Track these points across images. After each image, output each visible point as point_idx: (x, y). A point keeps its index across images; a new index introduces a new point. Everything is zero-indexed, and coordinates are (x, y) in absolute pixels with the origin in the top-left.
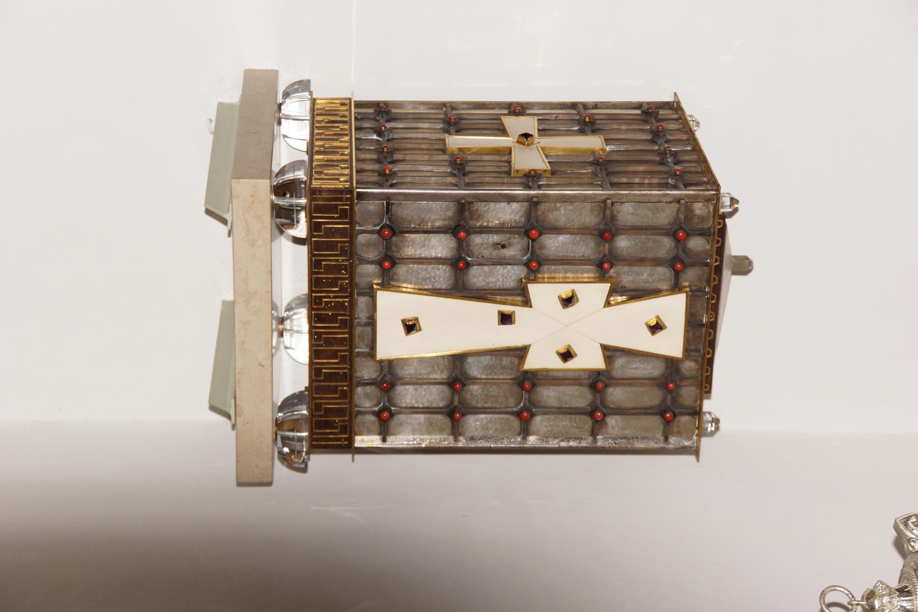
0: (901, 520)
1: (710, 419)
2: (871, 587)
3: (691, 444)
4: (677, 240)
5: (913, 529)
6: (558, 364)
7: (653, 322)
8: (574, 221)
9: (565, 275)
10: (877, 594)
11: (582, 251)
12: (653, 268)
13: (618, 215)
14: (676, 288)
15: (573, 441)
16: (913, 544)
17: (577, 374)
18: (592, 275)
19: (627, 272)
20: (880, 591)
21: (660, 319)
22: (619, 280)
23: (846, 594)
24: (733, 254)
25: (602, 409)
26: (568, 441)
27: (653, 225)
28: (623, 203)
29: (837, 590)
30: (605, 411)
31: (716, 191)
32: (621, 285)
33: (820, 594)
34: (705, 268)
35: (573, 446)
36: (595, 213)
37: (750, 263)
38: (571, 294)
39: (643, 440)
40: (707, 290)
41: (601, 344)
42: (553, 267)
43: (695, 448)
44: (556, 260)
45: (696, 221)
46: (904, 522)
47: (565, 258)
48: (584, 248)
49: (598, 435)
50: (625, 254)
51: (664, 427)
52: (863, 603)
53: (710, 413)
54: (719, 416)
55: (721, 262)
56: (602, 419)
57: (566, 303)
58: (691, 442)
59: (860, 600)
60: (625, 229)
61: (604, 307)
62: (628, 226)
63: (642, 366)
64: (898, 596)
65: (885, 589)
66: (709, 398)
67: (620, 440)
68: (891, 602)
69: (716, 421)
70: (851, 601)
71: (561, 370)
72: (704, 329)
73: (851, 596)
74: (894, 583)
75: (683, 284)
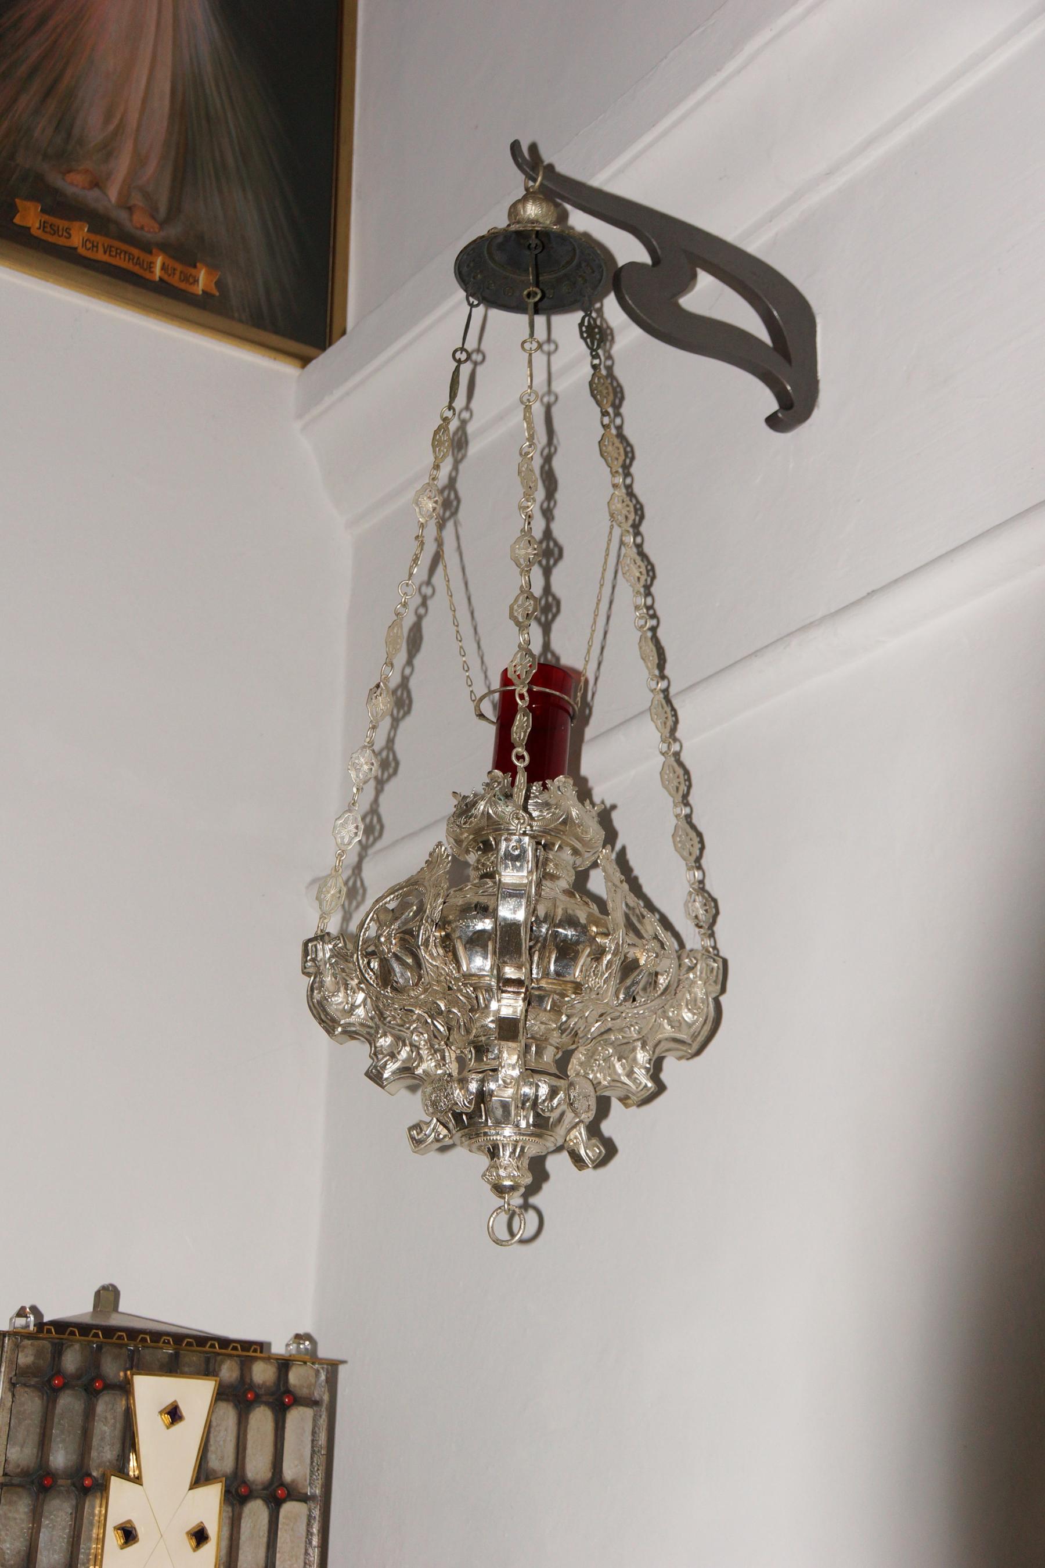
0: (415, 1147)
1: (295, 1345)
2: (489, 1187)
3: (323, 1371)
4: (64, 1386)
5: (425, 1135)
6: (210, 1550)
7: (167, 1418)
8: (23, 1528)
9: (93, 1540)
10: (497, 1182)
11: (64, 1517)
12: (96, 1418)
13: (21, 1467)
14: (126, 1389)
15: (312, 1528)
16: (441, 1136)
17: (227, 1521)
18: (98, 1502)
19: (99, 1453)
20: (494, 1178)
21: (165, 1409)
22: (108, 1464)
23: (496, 1216)
24: (91, 1309)
25: (274, 1486)
26: (312, 1534)
27: (39, 1419)
28: (6, 1461)
29: (493, 1225)
30: (276, 1484)
31: (5, 1337)
32: (115, 1462)
33: (496, 1245)
34: (104, 1350)
35: (317, 1528)
36: (15, 1498)
37: (104, 1288)
38: (119, 1531)
39: (316, 1433)
40: (132, 1348)
41: (190, 1489)
42: (81, 1556)
43: (330, 1367)
44: (72, 1553)
45: (42, 1362)
46: (417, 1143)
47: (71, 1540)
48: (61, 1513)
49: (307, 1494)
50: (74, 1457)
51: (302, 1405)
52: (507, 1198)
53: (288, 1345)
54: (291, 1335)
55: (97, 1327)
56: (286, 1488)
57: (131, 1538)
58: (322, 1371)
59: (503, 1201)
60: (41, 1457)
61: (142, 1485)
62: (38, 1453)
63: (222, 1434)
64: (499, 1159)
65: (491, 1172)
66: (269, 1344)
67: (314, 1464)
68: (506, 1167)
69: (298, 1337)
70: (505, 1210)
71: (218, 1544)
72: (181, 1352)
73: (499, 1211)
74: (484, 1161)
75: (121, 1378)
